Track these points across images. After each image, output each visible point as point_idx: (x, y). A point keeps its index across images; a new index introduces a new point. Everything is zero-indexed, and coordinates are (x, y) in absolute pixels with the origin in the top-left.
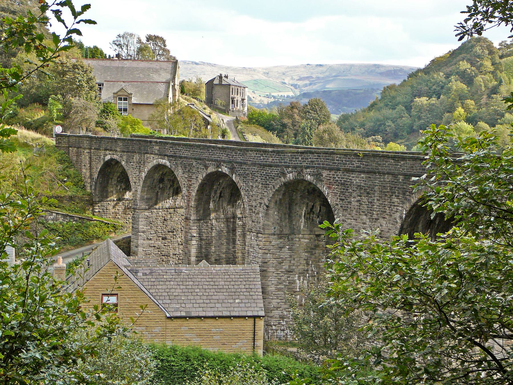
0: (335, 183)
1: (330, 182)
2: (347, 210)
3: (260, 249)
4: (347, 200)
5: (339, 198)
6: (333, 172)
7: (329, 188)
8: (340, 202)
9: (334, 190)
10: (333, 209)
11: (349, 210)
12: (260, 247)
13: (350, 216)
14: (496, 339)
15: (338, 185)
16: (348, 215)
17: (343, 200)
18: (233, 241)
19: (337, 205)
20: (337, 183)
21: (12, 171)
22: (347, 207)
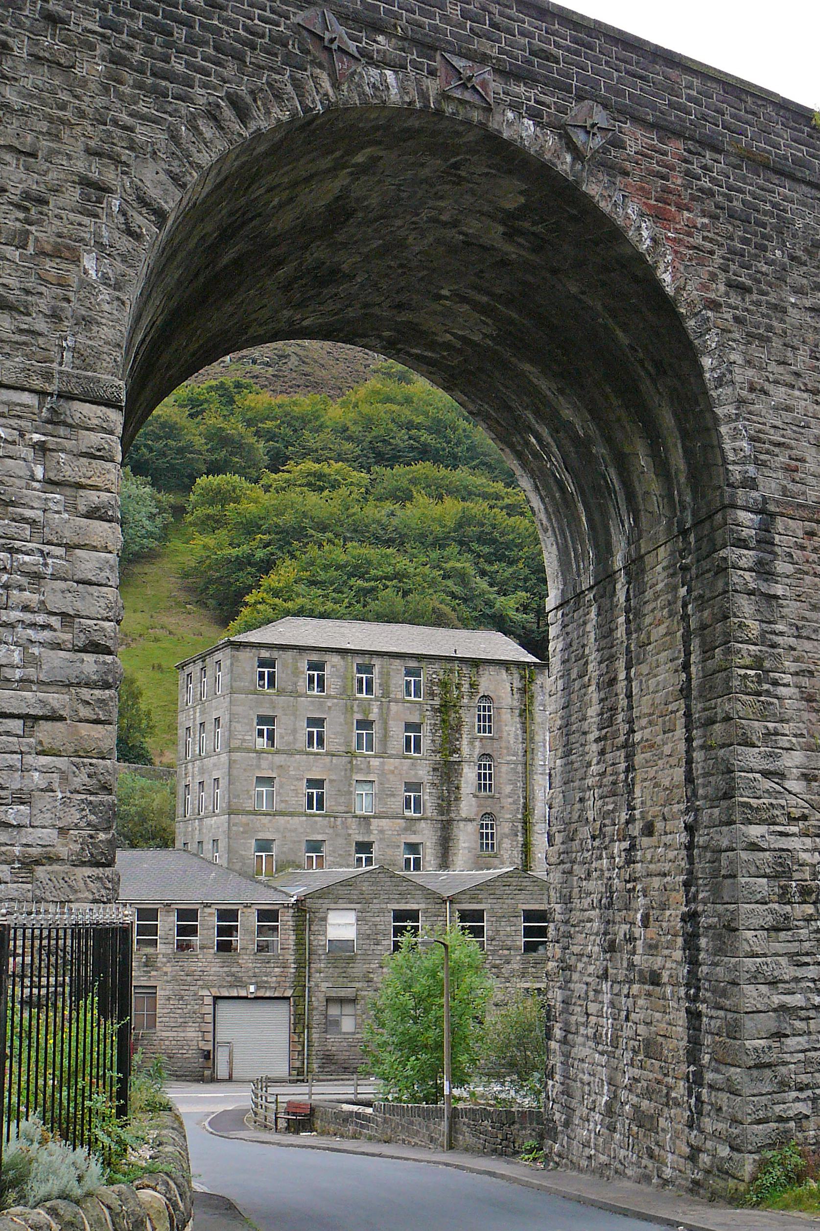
0: (693, 198)
1: (665, 190)
2: (769, 340)
3: (89, 515)
4: (765, 294)
5: (722, 276)
6: (675, 147)
7: (660, 217)
8: (727, 294)
9: (690, 235)
10: (692, 323)
11: (777, 343)
12: (94, 498)
13: (781, 369)
14: (13, 313)
15: (714, 217)
16: (773, 367)
17: (747, 290)
18: (222, 931)
19: (714, 305)
20: (711, 207)
21: (65, 220)
22: (769, 328)
